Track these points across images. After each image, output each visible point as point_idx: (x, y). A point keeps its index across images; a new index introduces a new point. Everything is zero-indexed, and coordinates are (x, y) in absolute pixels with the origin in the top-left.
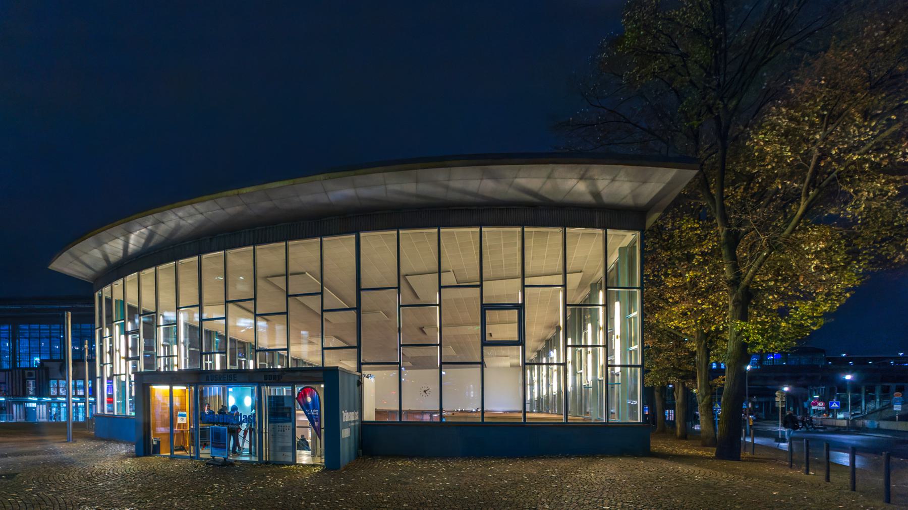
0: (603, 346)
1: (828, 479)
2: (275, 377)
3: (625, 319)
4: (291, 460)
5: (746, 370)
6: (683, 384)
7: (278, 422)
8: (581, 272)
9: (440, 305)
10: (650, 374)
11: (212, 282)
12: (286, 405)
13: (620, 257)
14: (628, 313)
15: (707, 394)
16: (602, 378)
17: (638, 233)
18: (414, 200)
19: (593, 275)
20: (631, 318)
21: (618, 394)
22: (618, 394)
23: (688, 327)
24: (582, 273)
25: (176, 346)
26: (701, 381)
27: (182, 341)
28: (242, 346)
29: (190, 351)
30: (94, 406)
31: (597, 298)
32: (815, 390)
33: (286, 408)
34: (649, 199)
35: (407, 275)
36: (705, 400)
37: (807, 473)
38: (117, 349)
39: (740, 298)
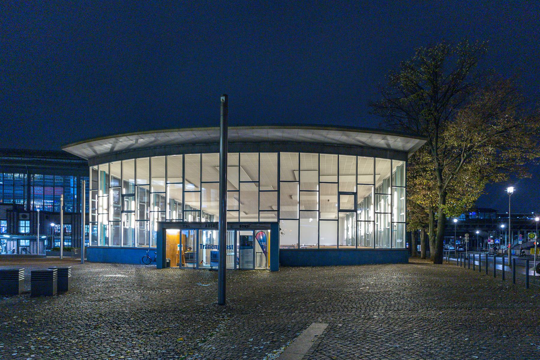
0: (390, 213)
1: (465, 267)
2: (245, 226)
3: (399, 200)
4: (252, 267)
5: (454, 223)
6: (424, 231)
7: (245, 249)
8: (379, 174)
9: (319, 191)
10: (409, 225)
11: (192, 171)
12: (249, 240)
13: (397, 169)
14: (400, 213)
15: (433, 236)
16: (389, 227)
17: (405, 162)
18: (309, 140)
19: (385, 176)
20: (401, 200)
21: (395, 235)
22: (395, 235)
23: (425, 203)
24: (380, 175)
25: (134, 201)
26: (431, 229)
27: (168, 203)
28: (164, 200)
29: (140, 205)
30: (125, 243)
31: (388, 191)
32: (491, 233)
33: (249, 242)
34: (408, 149)
35: (294, 170)
36: (432, 238)
37: (461, 266)
38: (101, 205)
39: (443, 194)
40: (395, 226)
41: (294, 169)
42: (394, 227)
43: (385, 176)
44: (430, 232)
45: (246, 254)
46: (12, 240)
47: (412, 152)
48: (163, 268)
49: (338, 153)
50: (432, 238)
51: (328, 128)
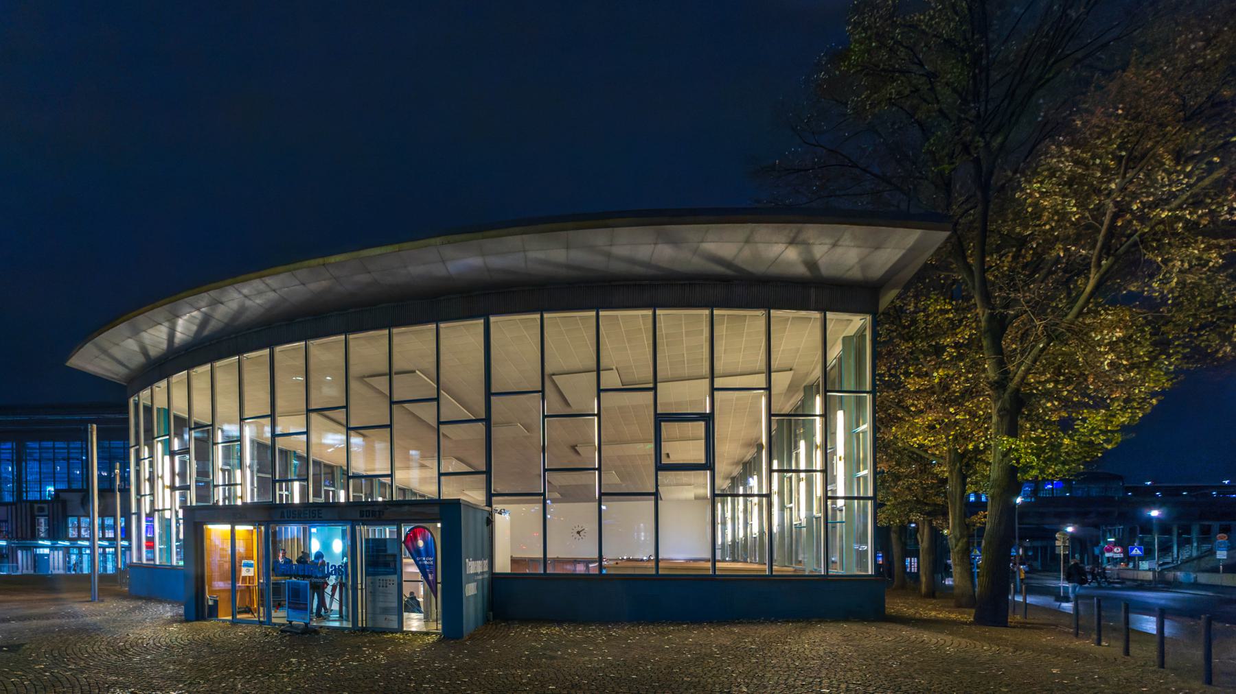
0: (821, 471)
2: (374, 513)
3: (851, 435)
8: (791, 370)
10: (885, 508)
12: (390, 552)
13: (843, 350)
15: (962, 536)
16: (820, 515)
17: (869, 318)
19: (807, 375)
20: (859, 433)
21: (841, 537)
22: (841, 537)
23: (937, 445)
24: (792, 372)
25: (240, 470)
26: (954, 519)
27: (248, 464)
29: (258, 477)
31: (813, 406)
32: (1110, 531)
33: (389, 555)
35: (554, 374)
36: (960, 544)
39: (1008, 406)
40: (841, 510)
41: (551, 372)
42: (838, 512)
43: (807, 375)
44: (954, 526)
45: (381, 588)
46: (56, 550)
47: (894, 287)
48: (197, 619)
49: (654, 305)
50: (960, 544)
51: (611, 221)
